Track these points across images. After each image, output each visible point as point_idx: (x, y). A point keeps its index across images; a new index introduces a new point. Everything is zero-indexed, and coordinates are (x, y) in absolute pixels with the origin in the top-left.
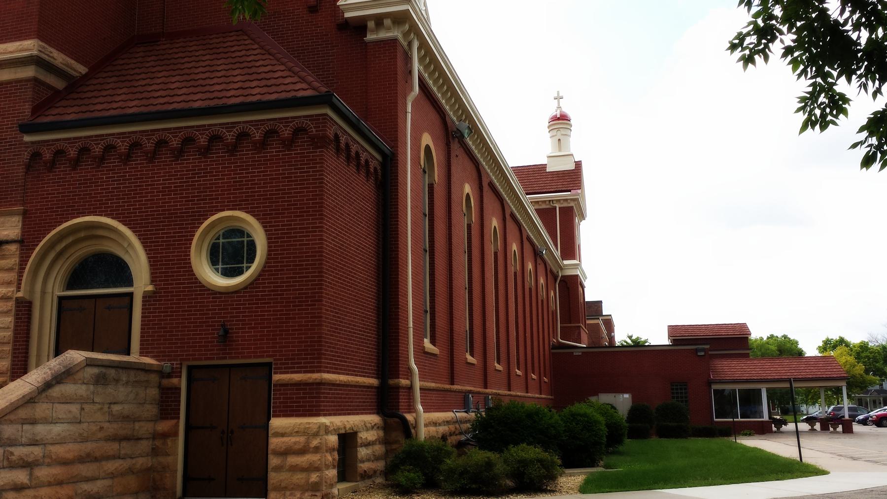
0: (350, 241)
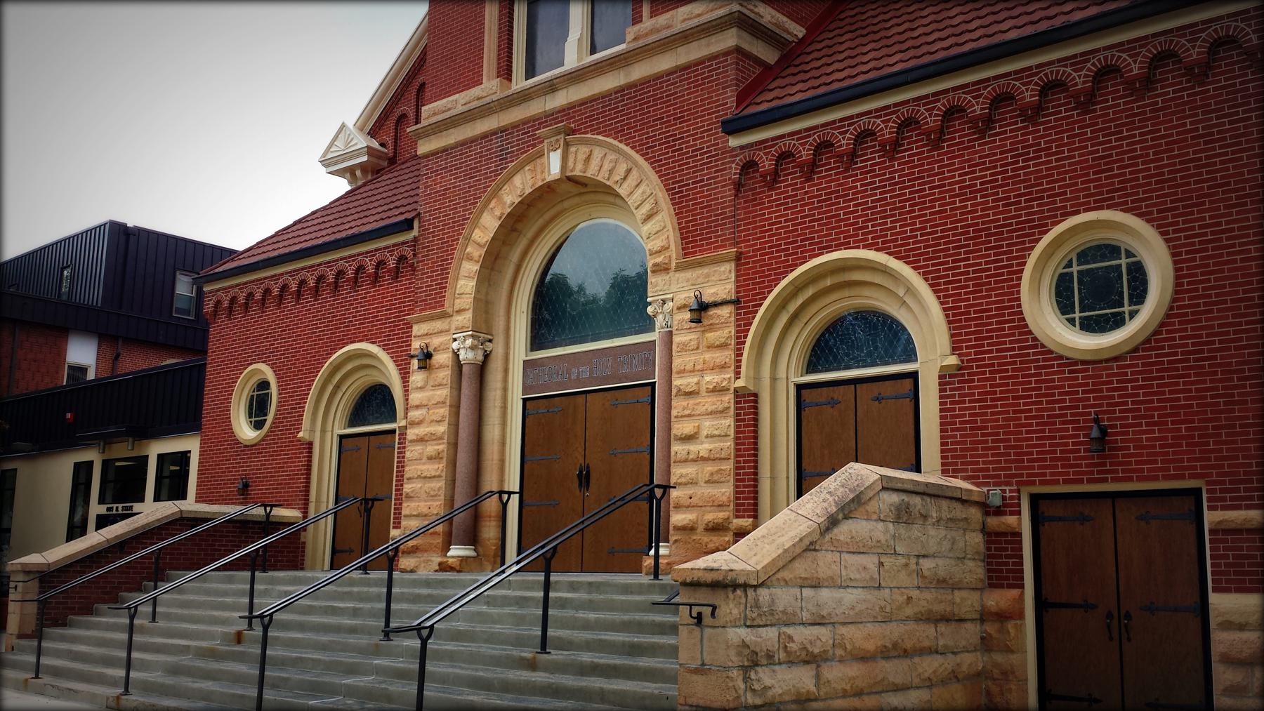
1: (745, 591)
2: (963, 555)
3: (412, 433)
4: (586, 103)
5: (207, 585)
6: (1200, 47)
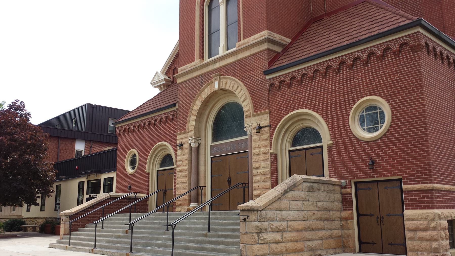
0: (442, 105)
1: (258, 212)
2: (333, 201)
3: (178, 169)
4: (225, 66)
6: (397, 46)
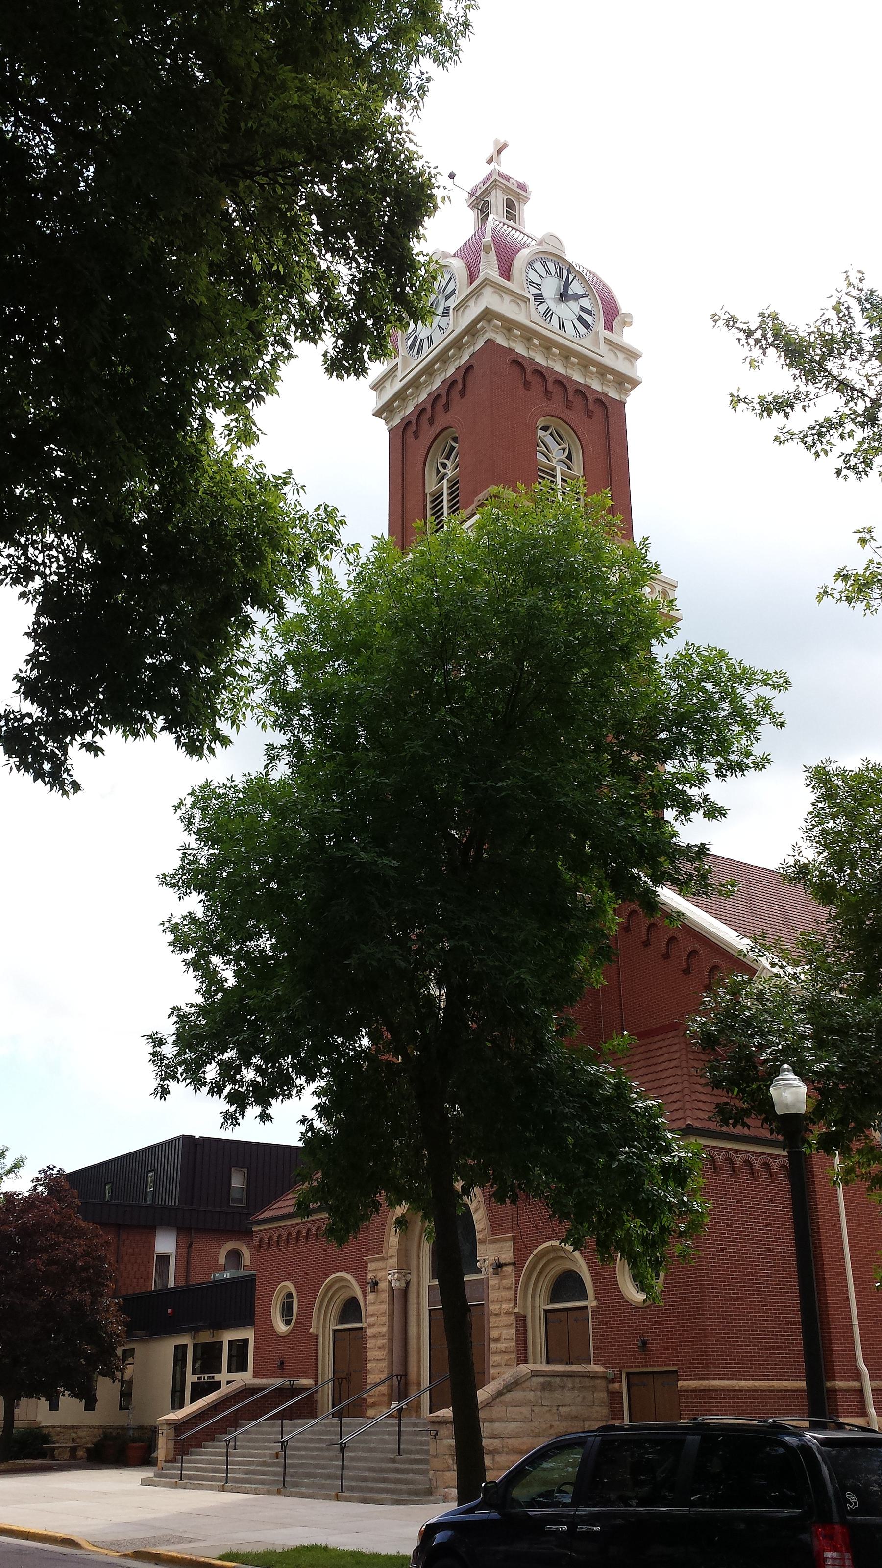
3: (370, 1332)
5: (261, 1429)
